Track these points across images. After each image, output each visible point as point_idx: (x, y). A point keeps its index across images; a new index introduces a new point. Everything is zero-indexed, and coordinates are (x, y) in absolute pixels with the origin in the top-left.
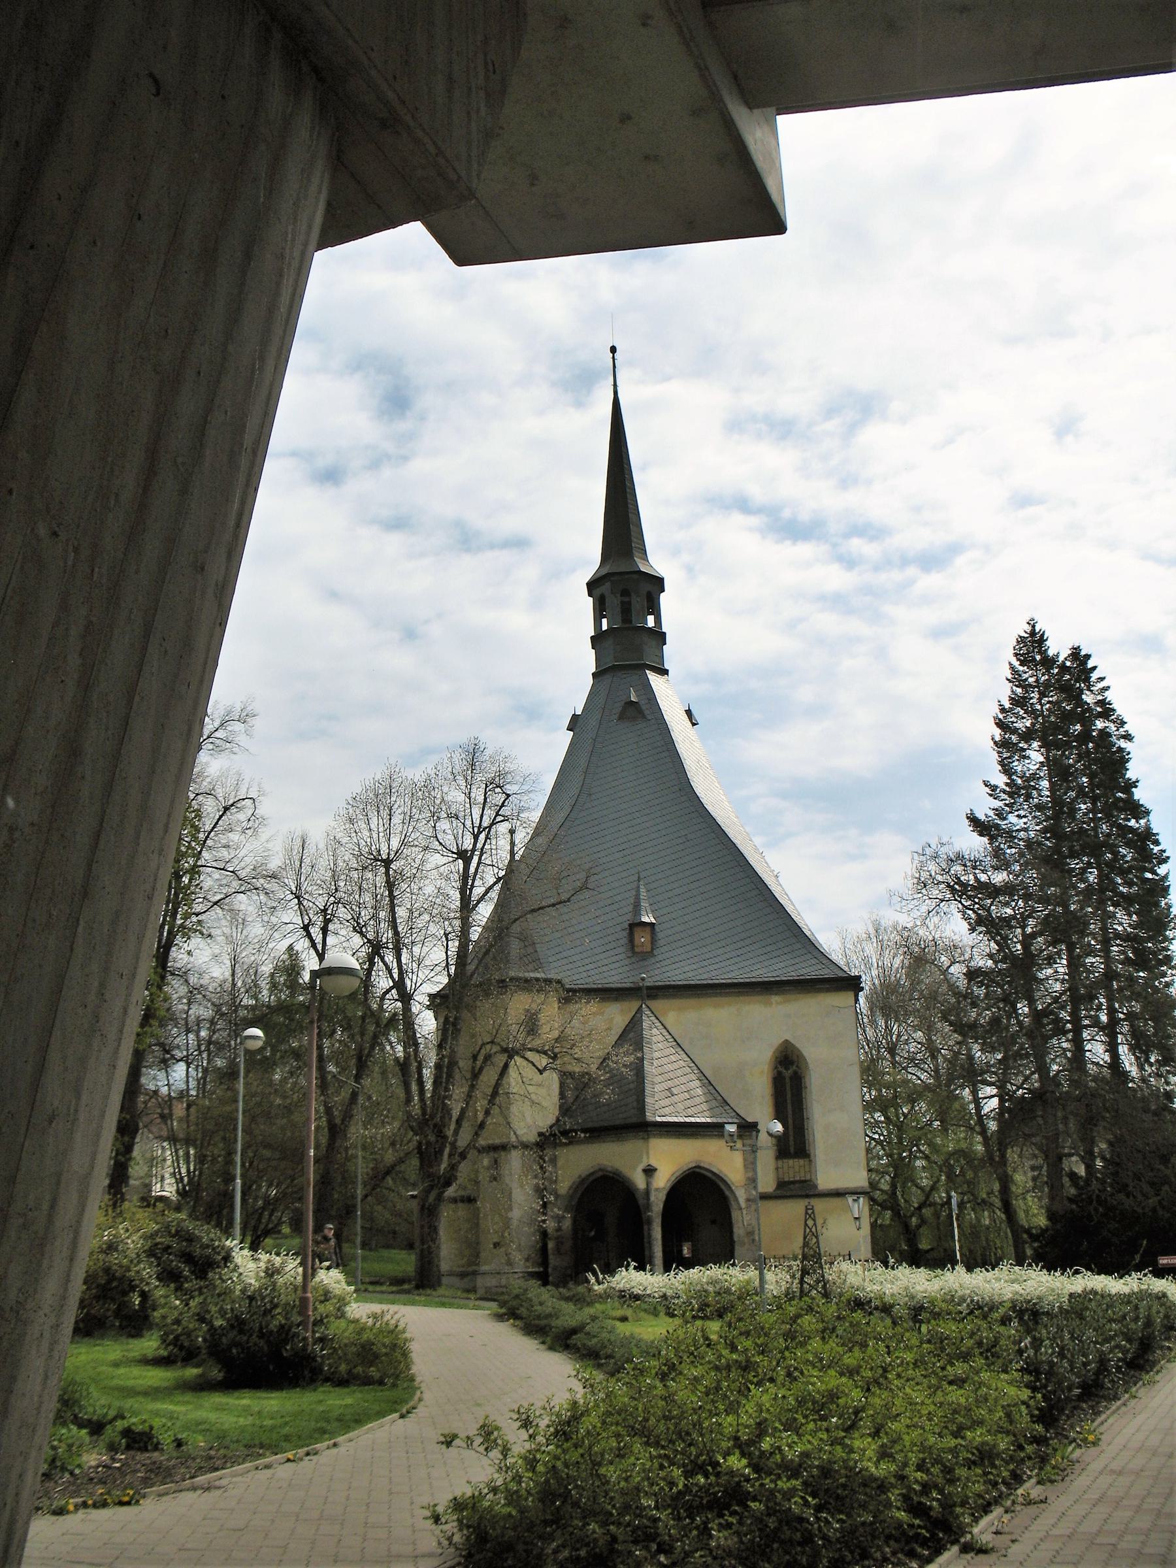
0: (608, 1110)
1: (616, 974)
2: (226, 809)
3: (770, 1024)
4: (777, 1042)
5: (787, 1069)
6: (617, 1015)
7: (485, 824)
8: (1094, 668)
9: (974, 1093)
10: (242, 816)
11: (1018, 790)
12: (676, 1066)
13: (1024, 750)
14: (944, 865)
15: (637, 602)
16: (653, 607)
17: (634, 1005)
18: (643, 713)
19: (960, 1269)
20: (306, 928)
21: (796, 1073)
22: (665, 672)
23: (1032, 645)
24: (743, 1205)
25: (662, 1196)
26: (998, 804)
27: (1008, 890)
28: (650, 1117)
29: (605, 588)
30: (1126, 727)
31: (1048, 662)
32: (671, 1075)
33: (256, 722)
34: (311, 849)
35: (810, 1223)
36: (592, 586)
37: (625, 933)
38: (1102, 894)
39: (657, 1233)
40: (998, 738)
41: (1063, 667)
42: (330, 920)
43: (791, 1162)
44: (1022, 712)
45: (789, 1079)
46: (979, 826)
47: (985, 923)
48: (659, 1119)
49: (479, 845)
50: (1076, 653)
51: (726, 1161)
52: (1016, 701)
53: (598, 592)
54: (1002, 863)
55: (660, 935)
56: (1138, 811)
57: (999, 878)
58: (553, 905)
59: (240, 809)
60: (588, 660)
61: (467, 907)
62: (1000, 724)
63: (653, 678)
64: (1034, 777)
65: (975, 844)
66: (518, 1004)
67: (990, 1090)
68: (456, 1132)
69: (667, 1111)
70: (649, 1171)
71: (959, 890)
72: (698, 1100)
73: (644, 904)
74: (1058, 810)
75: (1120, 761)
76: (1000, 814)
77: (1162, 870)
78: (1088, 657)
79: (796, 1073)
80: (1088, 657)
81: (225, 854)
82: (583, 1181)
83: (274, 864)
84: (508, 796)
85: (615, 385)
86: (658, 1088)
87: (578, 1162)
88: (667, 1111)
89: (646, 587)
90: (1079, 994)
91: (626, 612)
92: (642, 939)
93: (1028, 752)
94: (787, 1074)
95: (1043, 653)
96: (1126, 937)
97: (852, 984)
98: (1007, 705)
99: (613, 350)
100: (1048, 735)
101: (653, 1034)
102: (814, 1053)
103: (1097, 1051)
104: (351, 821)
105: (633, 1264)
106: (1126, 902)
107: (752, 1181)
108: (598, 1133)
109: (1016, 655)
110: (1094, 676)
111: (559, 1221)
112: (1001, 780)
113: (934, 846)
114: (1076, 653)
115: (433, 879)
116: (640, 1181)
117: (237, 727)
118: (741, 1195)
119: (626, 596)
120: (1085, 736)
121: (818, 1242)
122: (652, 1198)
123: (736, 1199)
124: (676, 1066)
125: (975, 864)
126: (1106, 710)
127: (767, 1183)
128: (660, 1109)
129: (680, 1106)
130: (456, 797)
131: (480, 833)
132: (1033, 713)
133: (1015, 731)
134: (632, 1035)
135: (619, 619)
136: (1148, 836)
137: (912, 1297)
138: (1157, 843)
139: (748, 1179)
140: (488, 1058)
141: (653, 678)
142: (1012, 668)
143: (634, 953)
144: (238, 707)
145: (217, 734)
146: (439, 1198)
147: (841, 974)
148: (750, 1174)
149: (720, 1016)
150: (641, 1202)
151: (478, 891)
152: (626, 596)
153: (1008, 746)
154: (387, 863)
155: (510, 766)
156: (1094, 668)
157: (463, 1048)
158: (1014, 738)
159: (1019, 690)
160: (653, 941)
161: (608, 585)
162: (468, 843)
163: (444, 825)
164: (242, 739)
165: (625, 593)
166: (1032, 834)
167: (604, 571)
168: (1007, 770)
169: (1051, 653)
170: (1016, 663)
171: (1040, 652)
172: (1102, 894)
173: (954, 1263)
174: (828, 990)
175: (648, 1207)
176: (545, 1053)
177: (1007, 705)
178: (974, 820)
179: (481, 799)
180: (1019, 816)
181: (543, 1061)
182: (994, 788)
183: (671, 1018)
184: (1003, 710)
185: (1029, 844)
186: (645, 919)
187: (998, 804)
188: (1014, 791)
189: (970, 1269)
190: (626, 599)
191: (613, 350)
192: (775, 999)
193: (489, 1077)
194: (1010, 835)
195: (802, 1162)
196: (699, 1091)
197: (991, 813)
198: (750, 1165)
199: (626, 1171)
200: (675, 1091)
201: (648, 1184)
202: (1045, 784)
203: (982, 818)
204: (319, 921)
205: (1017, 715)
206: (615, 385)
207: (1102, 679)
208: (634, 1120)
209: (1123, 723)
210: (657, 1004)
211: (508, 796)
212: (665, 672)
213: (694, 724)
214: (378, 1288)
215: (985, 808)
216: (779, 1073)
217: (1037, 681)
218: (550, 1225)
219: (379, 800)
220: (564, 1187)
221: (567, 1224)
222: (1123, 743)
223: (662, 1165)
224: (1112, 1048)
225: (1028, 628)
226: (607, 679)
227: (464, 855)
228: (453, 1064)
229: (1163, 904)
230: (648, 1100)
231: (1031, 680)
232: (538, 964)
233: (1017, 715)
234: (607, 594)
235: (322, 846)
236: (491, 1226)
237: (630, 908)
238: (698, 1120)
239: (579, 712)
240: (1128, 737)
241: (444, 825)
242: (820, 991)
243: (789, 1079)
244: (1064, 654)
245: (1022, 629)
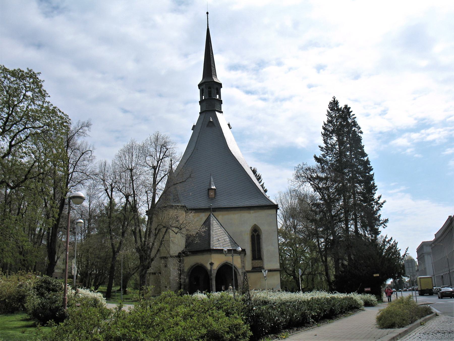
0: (200, 245)
1: (203, 205)
2: (83, 154)
3: (249, 220)
4: (252, 224)
5: (255, 233)
6: (203, 216)
7: (161, 158)
8: (352, 111)
9: (318, 241)
10: (88, 156)
11: (328, 149)
12: (220, 232)
13: (331, 136)
14: (305, 171)
15: (213, 91)
16: (219, 93)
17: (207, 214)
18: (216, 125)
19: (301, 292)
20: (106, 190)
21: (258, 234)
22: (221, 112)
23: (334, 105)
24: (241, 274)
25: (216, 272)
26: (323, 153)
27: (326, 179)
28: (212, 247)
29: (203, 87)
30: (361, 129)
31: (339, 110)
32: (219, 235)
33: (91, 127)
34: (107, 166)
35: (245, 278)
36: (200, 86)
37: (207, 192)
38: (353, 180)
39: (214, 283)
40: (323, 133)
41: (343, 111)
42: (113, 188)
43: (256, 261)
44: (331, 125)
45: (256, 236)
46: (318, 160)
47: (317, 189)
48: (214, 248)
49: (159, 164)
50: (346, 107)
51: (236, 261)
52: (329, 122)
53: (201, 88)
54: (323, 171)
55: (217, 192)
56: (364, 155)
57: (323, 175)
58: (181, 183)
59: (87, 154)
60: (198, 108)
61: (155, 183)
62: (324, 128)
63: (217, 113)
64: (334, 145)
65: (314, 164)
66: (172, 213)
67: (322, 240)
68: (150, 252)
69: (217, 245)
70: (212, 264)
71: (311, 179)
72: (227, 242)
73: (212, 183)
74: (341, 154)
75: (359, 140)
76: (324, 155)
77: (371, 173)
78: (350, 108)
79: (258, 234)
80: (350, 108)
81: (82, 168)
82: (192, 267)
83: (97, 171)
84: (167, 149)
85: (208, 26)
86: (214, 239)
87: (191, 261)
88: (217, 245)
89: (216, 86)
90: (347, 209)
91: (210, 94)
92: (212, 193)
93: (333, 137)
94: (256, 234)
95: (337, 107)
96: (361, 193)
97: (275, 207)
98: (326, 123)
99: (207, 13)
100: (338, 131)
101: (214, 224)
102: (264, 229)
103: (352, 228)
104: (120, 157)
105: (199, 291)
106: (360, 182)
107: (243, 267)
108: (195, 252)
109: (329, 108)
110: (351, 114)
111: (185, 279)
112: (324, 145)
113: (301, 165)
114: (346, 107)
115: (145, 175)
116: (209, 267)
117: (86, 128)
118: (240, 271)
119: (210, 91)
120: (348, 132)
121: (247, 283)
122: (212, 272)
123: (239, 272)
124: (220, 232)
125: (314, 171)
126: (355, 124)
127: (249, 267)
128: (215, 245)
129: (221, 244)
130: (152, 150)
131: (159, 161)
132: (334, 125)
133: (328, 131)
134: (207, 223)
135: (208, 96)
136: (368, 162)
137: (281, 300)
138: (369, 164)
139: (242, 266)
140: (159, 230)
141: (217, 113)
142: (328, 112)
143: (209, 198)
144: (86, 122)
145: (79, 131)
146: (146, 273)
147: (272, 204)
148: (243, 265)
149: (235, 217)
150: (209, 273)
151: (158, 179)
152: (210, 91)
153: (326, 135)
154: (131, 170)
155: (168, 140)
156: (352, 111)
157: (154, 226)
158: (328, 133)
159: (330, 118)
160: (215, 193)
161: (204, 85)
162: (155, 164)
163: (148, 158)
164: (87, 132)
165: (210, 88)
166: (333, 162)
167: (203, 81)
168: (326, 142)
169: (340, 107)
170: (329, 110)
171: (336, 107)
172: (353, 180)
173: (299, 290)
174: (268, 209)
175: (211, 275)
176: (178, 228)
177: (326, 123)
178: (315, 157)
179: (160, 150)
180: (329, 157)
181: (176, 230)
182: (322, 148)
183: (220, 218)
184: (325, 124)
185: (332, 165)
186: (213, 187)
187: (323, 153)
188: (327, 149)
189: (304, 292)
190: (210, 90)
191: (207, 13)
192: (252, 212)
193: (161, 235)
194: (326, 162)
195: (260, 261)
196: (228, 240)
197: (321, 156)
198: (243, 262)
199: (205, 265)
200: (220, 239)
201: (211, 268)
202: (337, 147)
203: (319, 157)
204: (109, 187)
205: (329, 126)
206: (208, 26)
207: (354, 115)
208: (207, 248)
209: (360, 128)
210: (216, 213)
211: (167, 149)
212: (221, 112)
213: (230, 128)
214: (128, 300)
215: (319, 154)
216: (253, 234)
217: (336, 115)
218: (182, 281)
219: (129, 150)
220: (186, 269)
221: (187, 280)
222: (360, 134)
223: (215, 262)
224: (356, 227)
225: (333, 100)
226: (204, 114)
227: (154, 168)
228: (150, 232)
229: (372, 183)
230: (211, 242)
231: (334, 115)
232: (178, 201)
233: (329, 126)
234: (204, 88)
235: (110, 165)
236: (163, 281)
237: (208, 184)
238: (220, 248)
239: (195, 125)
240: (361, 132)
241: (148, 158)
242: (265, 209)
243: (256, 236)
244: (343, 107)
245: (331, 100)
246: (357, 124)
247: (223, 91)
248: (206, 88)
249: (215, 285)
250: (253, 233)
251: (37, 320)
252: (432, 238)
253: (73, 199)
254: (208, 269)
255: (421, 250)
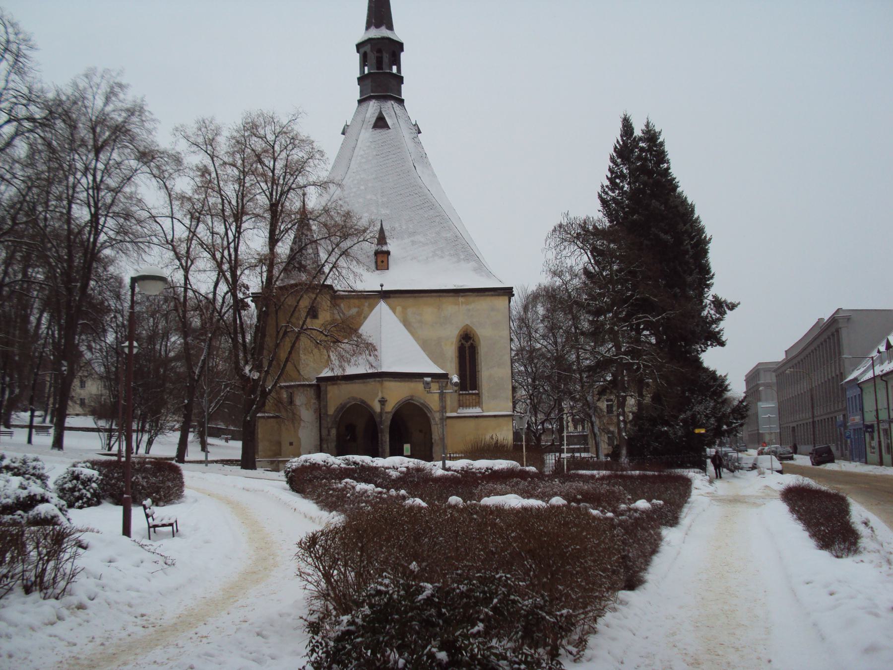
16: (397, 61)
25: (390, 416)
29: (367, 48)
45: (468, 350)
53: (362, 50)
94: (467, 345)
116: (377, 407)
118: (437, 416)
123: (434, 419)
150: (378, 420)
165: (379, 51)
175: (381, 423)
192: (461, 299)
199: (370, 403)
216: (462, 344)
220: (331, 411)
243: (468, 350)
246: (35, 495)
247: (405, 57)
248: (372, 51)
249: (388, 443)
250: (463, 342)
251: (181, 419)
252: (778, 356)
253: (141, 283)
254: (375, 412)
255: (753, 378)
